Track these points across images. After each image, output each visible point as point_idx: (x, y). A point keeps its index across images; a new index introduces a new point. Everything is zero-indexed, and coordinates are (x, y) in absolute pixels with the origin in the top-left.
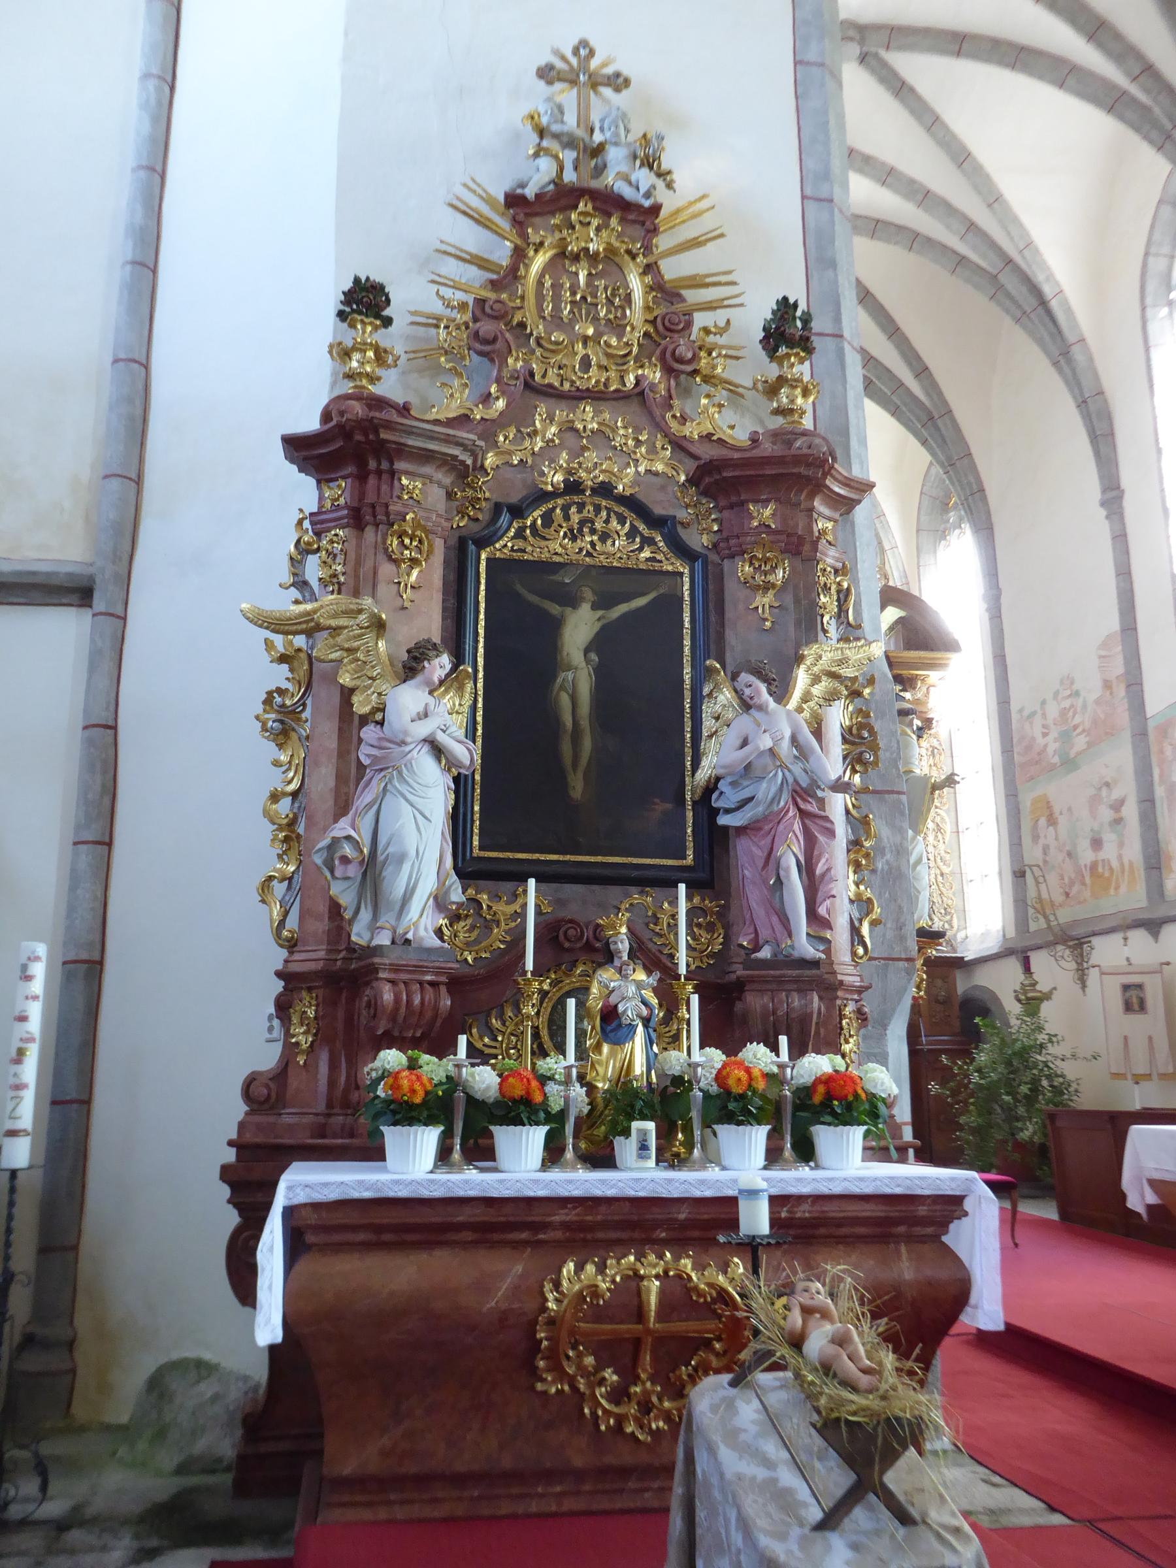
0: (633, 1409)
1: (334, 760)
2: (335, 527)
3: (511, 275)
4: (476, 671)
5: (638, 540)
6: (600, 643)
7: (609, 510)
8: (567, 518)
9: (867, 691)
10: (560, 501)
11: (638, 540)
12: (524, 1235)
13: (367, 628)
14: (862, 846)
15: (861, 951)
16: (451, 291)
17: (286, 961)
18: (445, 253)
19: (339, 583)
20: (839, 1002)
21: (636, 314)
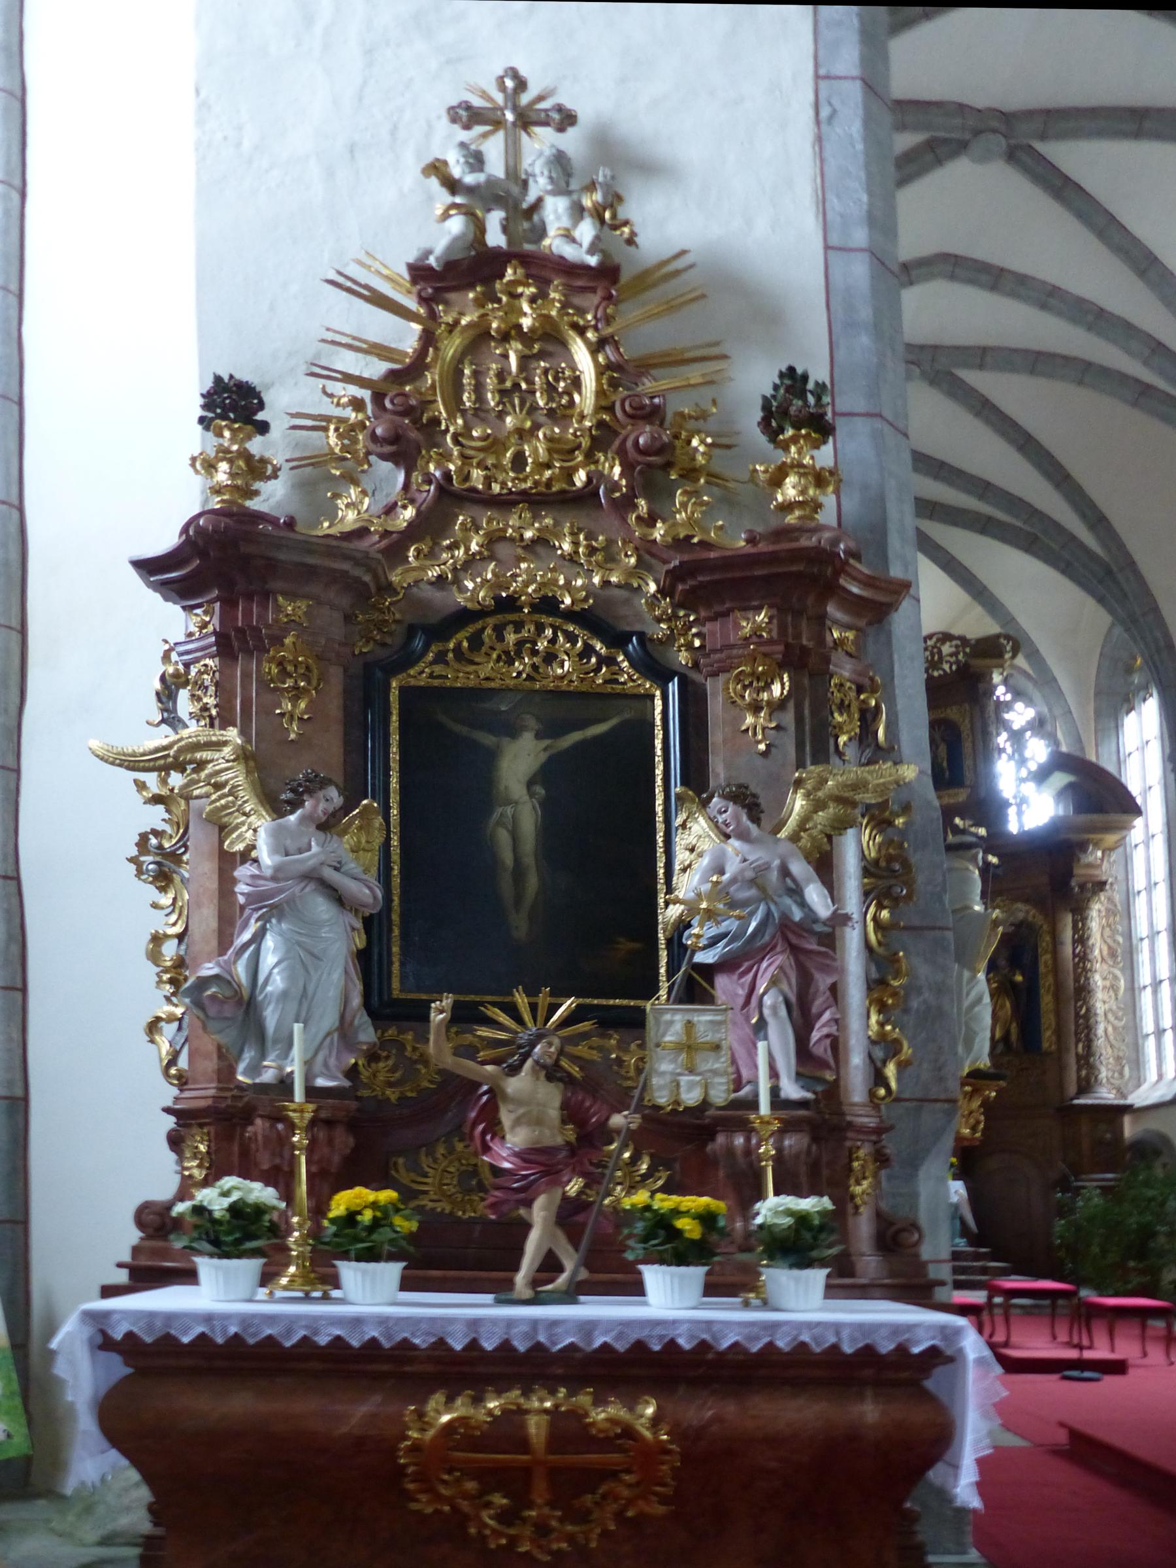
0: (528, 1531)
1: (216, 901)
2: (204, 657)
4: (387, 808)
5: (593, 660)
6: (547, 776)
7: (555, 629)
8: (501, 638)
9: (900, 821)
10: (491, 621)
11: (593, 660)
12: (385, 1367)
13: (233, 761)
14: (888, 985)
15: (882, 1092)
16: (340, 385)
17: (176, 1099)
18: (333, 343)
19: (210, 717)
20: (848, 1144)
21: (586, 399)
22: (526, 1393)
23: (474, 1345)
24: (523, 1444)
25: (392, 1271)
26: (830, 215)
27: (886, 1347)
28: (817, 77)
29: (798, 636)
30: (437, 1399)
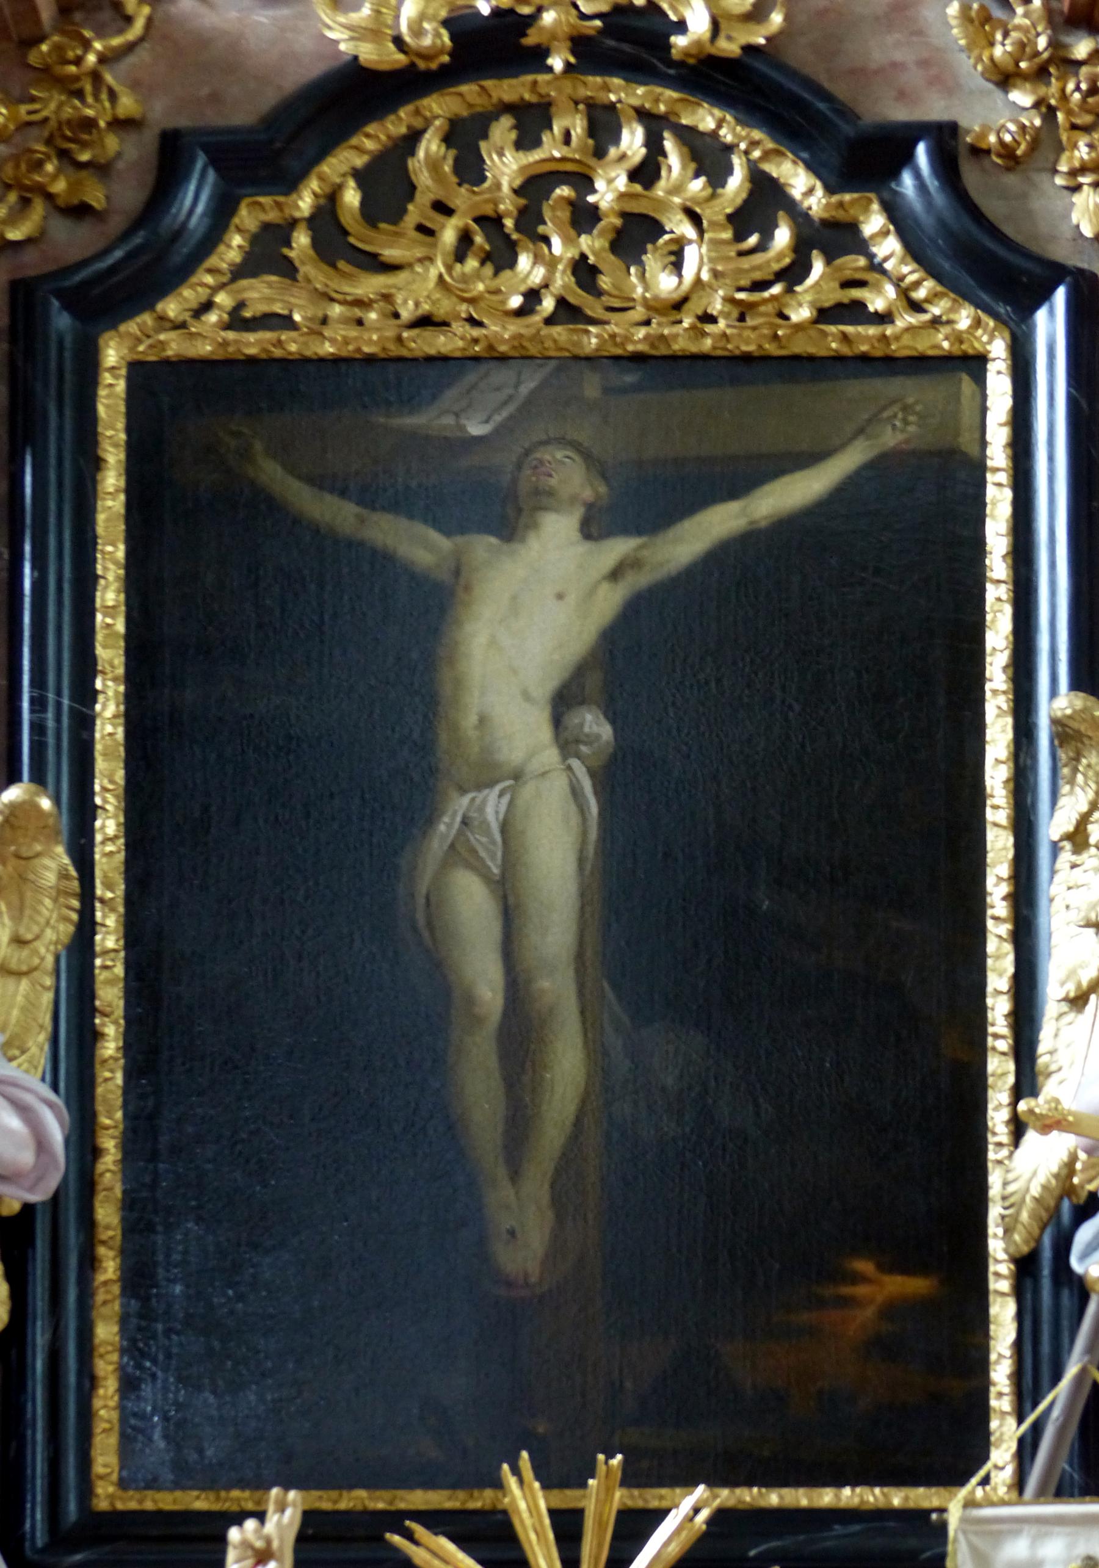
10: (439, 107)
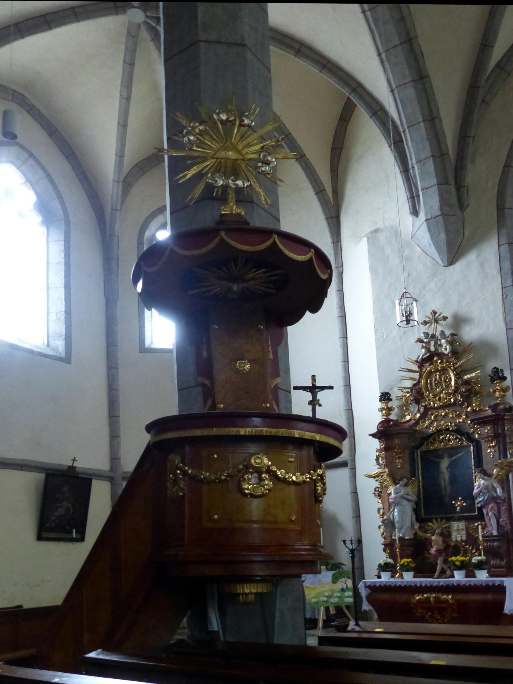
3: (419, 382)
10: (436, 435)
21: (453, 383)
22: (431, 594)
23: (421, 585)
24: (430, 602)
25: (411, 574)
26: (507, 321)
27: (491, 584)
28: (502, 288)
29: (498, 431)
30: (416, 595)
